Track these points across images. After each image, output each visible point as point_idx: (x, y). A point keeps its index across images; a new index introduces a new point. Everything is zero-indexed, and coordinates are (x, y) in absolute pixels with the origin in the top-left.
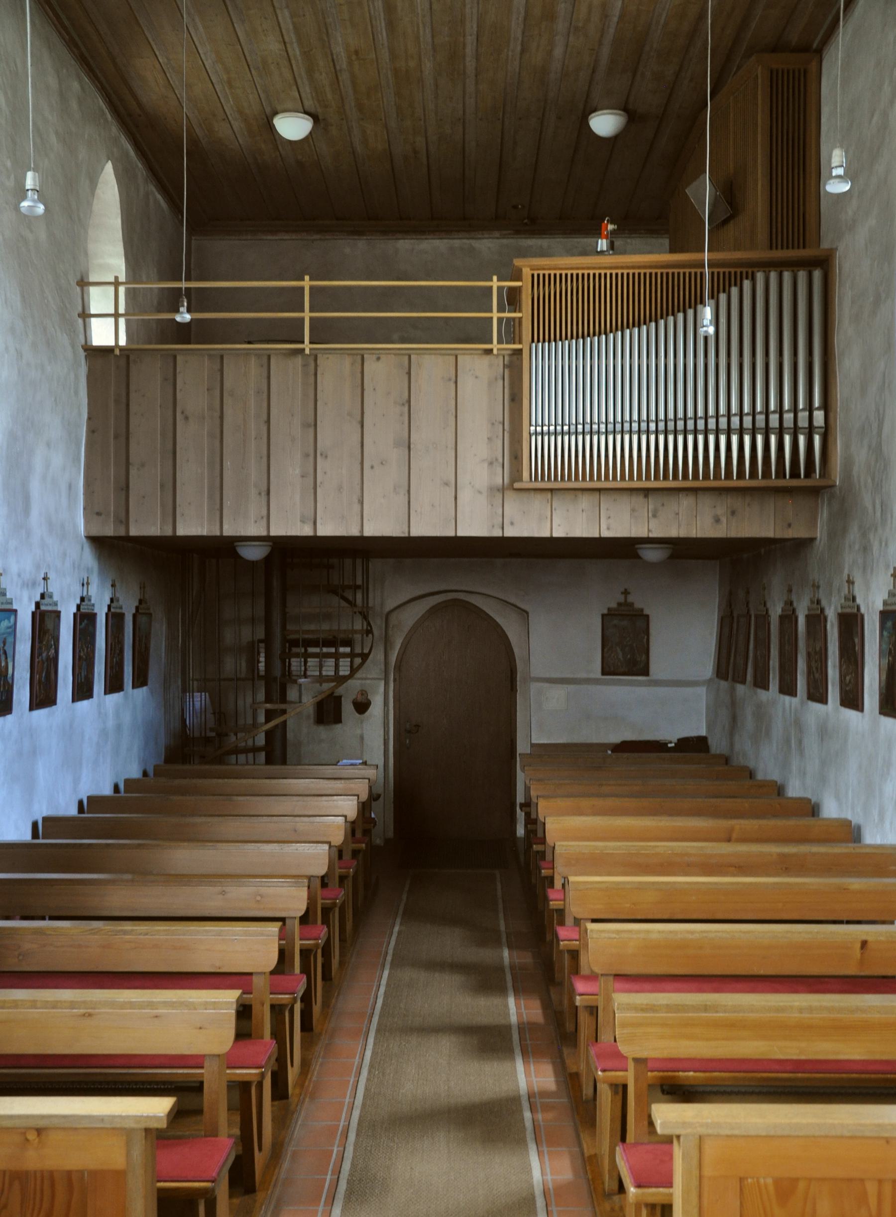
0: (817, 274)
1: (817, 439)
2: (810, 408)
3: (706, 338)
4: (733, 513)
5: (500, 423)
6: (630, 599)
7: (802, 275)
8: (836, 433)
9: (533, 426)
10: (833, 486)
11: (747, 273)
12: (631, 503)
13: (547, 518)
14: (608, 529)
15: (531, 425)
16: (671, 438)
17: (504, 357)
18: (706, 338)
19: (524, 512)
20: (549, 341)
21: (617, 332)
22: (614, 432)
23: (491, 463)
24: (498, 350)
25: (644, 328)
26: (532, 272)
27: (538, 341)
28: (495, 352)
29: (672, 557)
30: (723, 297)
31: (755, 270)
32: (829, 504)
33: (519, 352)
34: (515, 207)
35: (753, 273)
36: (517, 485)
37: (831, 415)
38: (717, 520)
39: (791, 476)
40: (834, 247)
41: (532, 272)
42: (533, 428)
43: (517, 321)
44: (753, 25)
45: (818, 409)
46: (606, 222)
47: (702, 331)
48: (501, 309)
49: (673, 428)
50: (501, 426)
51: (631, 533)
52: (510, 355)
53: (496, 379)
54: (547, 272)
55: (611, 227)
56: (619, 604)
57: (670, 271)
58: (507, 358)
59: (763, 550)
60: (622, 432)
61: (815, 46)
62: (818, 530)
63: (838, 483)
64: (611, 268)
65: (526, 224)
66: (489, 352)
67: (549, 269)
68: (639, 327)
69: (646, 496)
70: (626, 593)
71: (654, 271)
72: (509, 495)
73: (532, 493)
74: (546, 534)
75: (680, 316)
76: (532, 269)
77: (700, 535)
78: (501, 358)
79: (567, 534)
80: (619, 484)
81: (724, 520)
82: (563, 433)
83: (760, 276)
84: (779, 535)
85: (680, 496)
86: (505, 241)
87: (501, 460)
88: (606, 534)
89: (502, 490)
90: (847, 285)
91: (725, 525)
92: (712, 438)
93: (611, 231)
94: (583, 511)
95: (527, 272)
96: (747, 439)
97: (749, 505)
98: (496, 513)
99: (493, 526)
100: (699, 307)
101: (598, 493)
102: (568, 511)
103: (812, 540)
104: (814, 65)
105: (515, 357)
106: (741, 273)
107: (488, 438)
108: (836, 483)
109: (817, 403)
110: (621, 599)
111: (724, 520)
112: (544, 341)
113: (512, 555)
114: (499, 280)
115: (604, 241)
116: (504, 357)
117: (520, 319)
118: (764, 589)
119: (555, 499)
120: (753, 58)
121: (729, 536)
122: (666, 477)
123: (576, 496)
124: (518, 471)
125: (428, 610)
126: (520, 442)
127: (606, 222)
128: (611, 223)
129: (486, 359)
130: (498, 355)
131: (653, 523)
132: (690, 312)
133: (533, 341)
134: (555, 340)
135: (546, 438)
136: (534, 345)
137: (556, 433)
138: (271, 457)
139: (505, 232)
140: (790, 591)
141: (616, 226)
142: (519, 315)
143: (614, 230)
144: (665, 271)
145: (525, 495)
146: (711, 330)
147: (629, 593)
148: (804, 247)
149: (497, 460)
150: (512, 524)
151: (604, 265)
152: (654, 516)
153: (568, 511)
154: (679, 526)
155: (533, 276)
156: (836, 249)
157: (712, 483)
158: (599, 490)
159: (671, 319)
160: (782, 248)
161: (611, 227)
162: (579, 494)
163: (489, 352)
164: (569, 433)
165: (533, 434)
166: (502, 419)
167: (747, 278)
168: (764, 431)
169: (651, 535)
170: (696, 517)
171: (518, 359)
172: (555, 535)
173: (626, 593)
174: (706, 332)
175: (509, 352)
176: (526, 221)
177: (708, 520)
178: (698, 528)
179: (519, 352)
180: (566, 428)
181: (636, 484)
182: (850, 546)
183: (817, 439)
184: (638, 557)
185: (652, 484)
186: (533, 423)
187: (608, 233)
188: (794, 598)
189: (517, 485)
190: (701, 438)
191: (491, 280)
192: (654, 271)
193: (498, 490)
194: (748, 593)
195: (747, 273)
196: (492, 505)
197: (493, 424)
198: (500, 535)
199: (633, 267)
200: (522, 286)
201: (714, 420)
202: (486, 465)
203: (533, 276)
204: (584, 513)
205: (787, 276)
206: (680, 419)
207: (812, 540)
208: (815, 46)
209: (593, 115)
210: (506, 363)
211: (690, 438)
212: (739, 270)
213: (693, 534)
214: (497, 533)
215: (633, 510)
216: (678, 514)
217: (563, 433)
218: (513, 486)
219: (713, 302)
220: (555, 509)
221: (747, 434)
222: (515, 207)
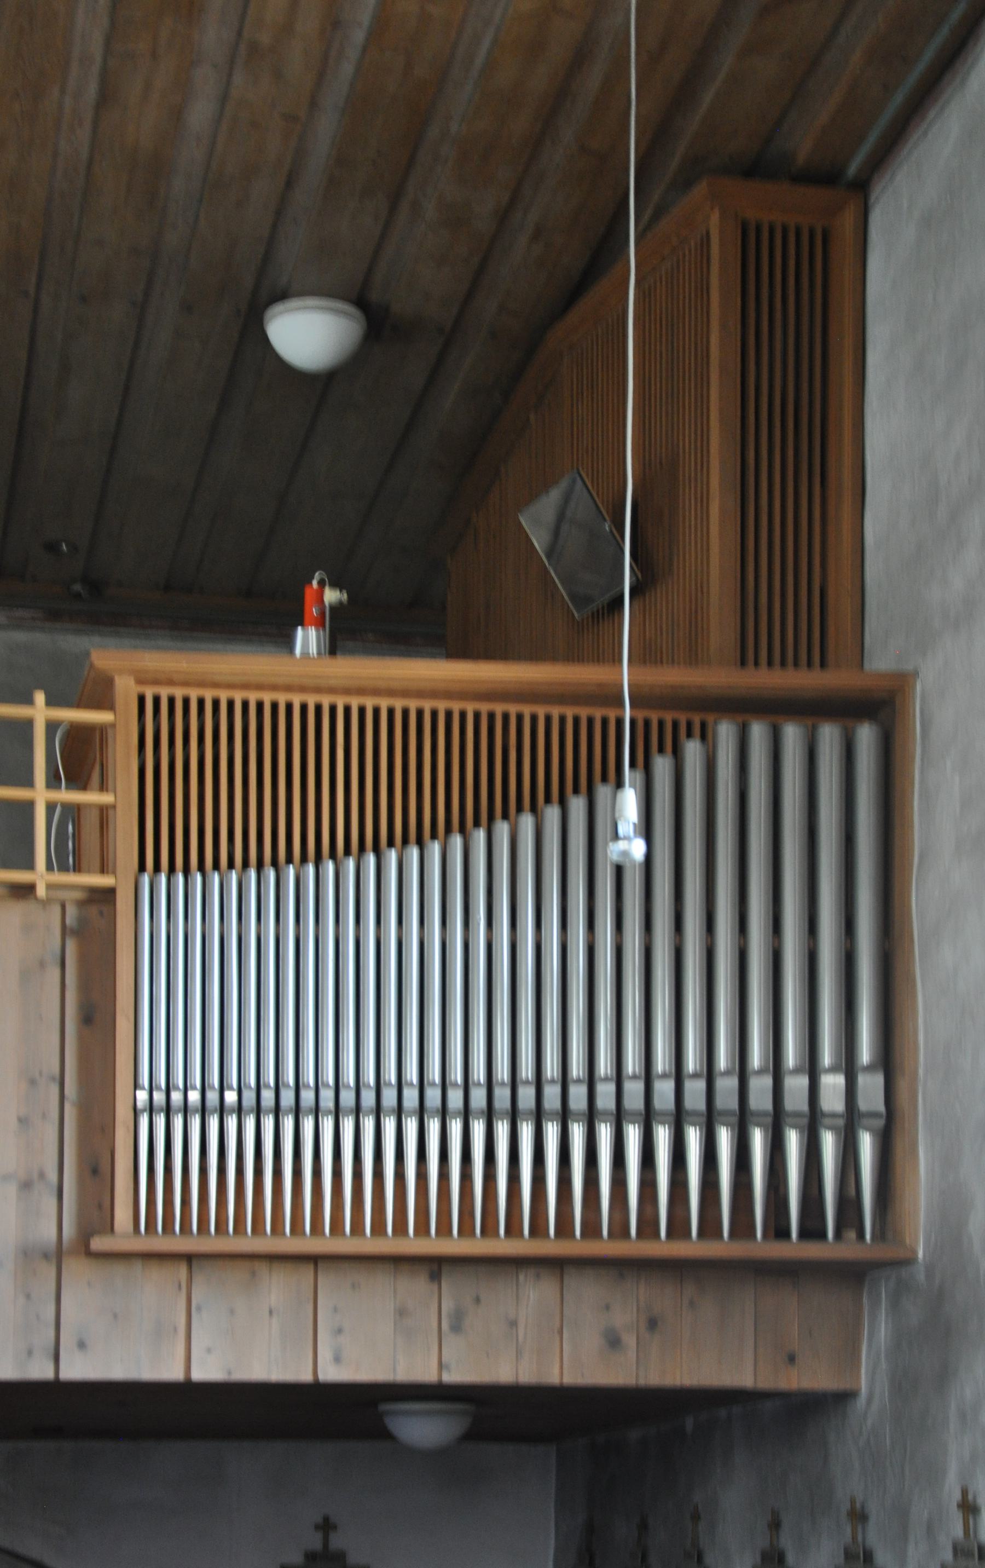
0: (866, 735)
1: (866, 1144)
2: (849, 1066)
3: (619, 870)
4: (653, 1324)
5: (53, 1079)
6: (337, 1541)
7: (829, 735)
8: (917, 1130)
9: (143, 1088)
10: (909, 1261)
11: (689, 725)
12: (395, 1292)
13: (175, 1330)
14: (337, 1359)
15: (136, 1086)
16: (502, 1130)
17: (63, 907)
18: (619, 870)
19: (115, 1316)
20: (186, 871)
21: (366, 857)
22: (357, 1111)
23: (26, 1185)
24: (50, 887)
25: (435, 849)
26: (141, 689)
27: (157, 869)
28: (41, 891)
29: (472, 1435)
30: (662, 766)
31: (710, 719)
32: (895, 1304)
33: (109, 894)
34: (52, 547)
35: (703, 726)
36: (98, 1244)
37: (902, 1085)
38: (613, 1341)
39: (804, 1234)
40: (909, 667)
41: (141, 689)
42: (142, 1096)
43: (90, 823)
44: (707, 98)
45: (870, 1068)
46: (315, 583)
47: (615, 850)
48: (53, 781)
49: (507, 1104)
50: (55, 1089)
51: (394, 1369)
52: (81, 904)
53: (42, 965)
54: (179, 693)
55: (331, 596)
56: (311, 1557)
57: (499, 709)
58: (71, 911)
59: (689, 1423)
60: (378, 1111)
61: (852, 170)
62: (863, 1371)
63: (920, 1254)
64: (347, 691)
65: (78, 596)
66: (24, 891)
67: (186, 684)
68: (420, 843)
69: (435, 1277)
70: (326, 1526)
71: (456, 707)
72: (75, 1269)
73: (138, 1266)
74: (172, 1372)
75: (552, 814)
76: (140, 682)
77: (569, 1379)
78: (57, 910)
79: (229, 1373)
80: (369, 1245)
81: (630, 1341)
82: (222, 1110)
83: (725, 732)
84: (766, 1382)
85: (521, 1277)
86: (20, 636)
87: (53, 1176)
88: (330, 1373)
89: (58, 1255)
90: (949, 764)
91: (632, 1354)
92: (605, 1133)
93: (332, 608)
94: (271, 1312)
95: (126, 689)
96: (693, 1138)
97: (692, 1304)
98: (38, 1317)
99: (30, 1353)
100: (603, 792)
101: (312, 1266)
102: (232, 1312)
103: (844, 1398)
104: (848, 220)
105: (93, 910)
106: (675, 725)
107: (20, 1120)
108: (915, 1252)
109: (865, 1054)
110: (315, 1542)
111: (630, 1341)
112: (172, 869)
113: (40, 1432)
114: (50, 703)
115: (312, 632)
116: (63, 907)
117: (104, 812)
118: (696, 1517)
119: (198, 1280)
120: (701, 189)
121: (642, 1382)
122: (489, 1228)
123: (253, 1274)
124: (100, 1206)
125: (345, 1557)
126: (108, 1130)
127: (315, 583)
128: (335, 584)
129: (15, 912)
130: (45, 903)
131: (454, 1348)
132: (577, 805)
133: (142, 868)
134: (186, 871)
135: (178, 1122)
136: (146, 879)
137: (203, 1111)
138: (98, 822)
139: (19, 613)
140: (775, 1525)
141: (345, 597)
142: (107, 798)
143: (341, 603)
144: (484, 708)
145: (119, 1270)
146: (638, 849)
147: (335, 1527)
148: (823, 664)
149: (42, 1175)
150: (82, 1345)
151: (333, 682)
152: (457, 1327)
153: (232, 1312)
154: (519, 1353)
155: (141, 700)
156: (916, 674)
157: (605, 1247)
158: (315, 1260)
159: (457, 841)
160: (770, 663)
161: (331, 596)
162: (262, 1268)
163: (24, 891)
164: (240, 1110)
165: (144, 1110)
166: (56, 1070)
167: (661, 750)
168: (735, 1120)
169: (448, 1378)
170: (561, 1332)
171: (101, 913)
172: (198, 1375)
173: (326, 1526)
174: (625, 854)
175: (78, 895)
176: (77, 587)
177: (592, 1341)
178: (565, 1359)
179: (109, 894)
180: (231, 1097)
181: (412, 1245)
182: (963, 1416)
183: (866, 1144)
184: (385, 1435)
185: (455, 1246)
186: (145, 1080)
187: (323, 614)
188: (786, 1542)
189: (98, 1244)
190: (577, 1133)
191: (29, 701)
192: (456, 707)
193: (46, 1256)
194: (643, 1526)
195: (689, 725)
196: (28, 1296)
197: (33, 1082)
198: (48, 1374)
199: (405, 693)
200: (113, 725)
201: (611, 1088)
202: (11, 1190)
203: (141, 700)
204: (275, 1320)
205: (792, 734)
206: (527, 1082)
207: (844, 1398)
208: (852, 170)
209: (278, 308)
210: (68, 921)
211: (552, 1132)
212: (668, 718)
213: (553, 1377)
214: (41, 1371)
215: (401, 1312)
216: (513, 1324)
217: (222, 1110)
218: (87, 1245)
219: (639, 776)
220: (199, 1309)
221: (694, 1125)
222: (52, 547)
